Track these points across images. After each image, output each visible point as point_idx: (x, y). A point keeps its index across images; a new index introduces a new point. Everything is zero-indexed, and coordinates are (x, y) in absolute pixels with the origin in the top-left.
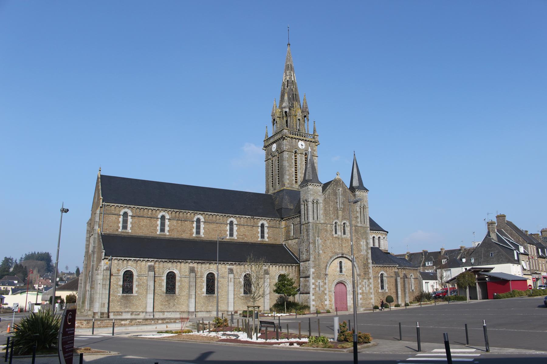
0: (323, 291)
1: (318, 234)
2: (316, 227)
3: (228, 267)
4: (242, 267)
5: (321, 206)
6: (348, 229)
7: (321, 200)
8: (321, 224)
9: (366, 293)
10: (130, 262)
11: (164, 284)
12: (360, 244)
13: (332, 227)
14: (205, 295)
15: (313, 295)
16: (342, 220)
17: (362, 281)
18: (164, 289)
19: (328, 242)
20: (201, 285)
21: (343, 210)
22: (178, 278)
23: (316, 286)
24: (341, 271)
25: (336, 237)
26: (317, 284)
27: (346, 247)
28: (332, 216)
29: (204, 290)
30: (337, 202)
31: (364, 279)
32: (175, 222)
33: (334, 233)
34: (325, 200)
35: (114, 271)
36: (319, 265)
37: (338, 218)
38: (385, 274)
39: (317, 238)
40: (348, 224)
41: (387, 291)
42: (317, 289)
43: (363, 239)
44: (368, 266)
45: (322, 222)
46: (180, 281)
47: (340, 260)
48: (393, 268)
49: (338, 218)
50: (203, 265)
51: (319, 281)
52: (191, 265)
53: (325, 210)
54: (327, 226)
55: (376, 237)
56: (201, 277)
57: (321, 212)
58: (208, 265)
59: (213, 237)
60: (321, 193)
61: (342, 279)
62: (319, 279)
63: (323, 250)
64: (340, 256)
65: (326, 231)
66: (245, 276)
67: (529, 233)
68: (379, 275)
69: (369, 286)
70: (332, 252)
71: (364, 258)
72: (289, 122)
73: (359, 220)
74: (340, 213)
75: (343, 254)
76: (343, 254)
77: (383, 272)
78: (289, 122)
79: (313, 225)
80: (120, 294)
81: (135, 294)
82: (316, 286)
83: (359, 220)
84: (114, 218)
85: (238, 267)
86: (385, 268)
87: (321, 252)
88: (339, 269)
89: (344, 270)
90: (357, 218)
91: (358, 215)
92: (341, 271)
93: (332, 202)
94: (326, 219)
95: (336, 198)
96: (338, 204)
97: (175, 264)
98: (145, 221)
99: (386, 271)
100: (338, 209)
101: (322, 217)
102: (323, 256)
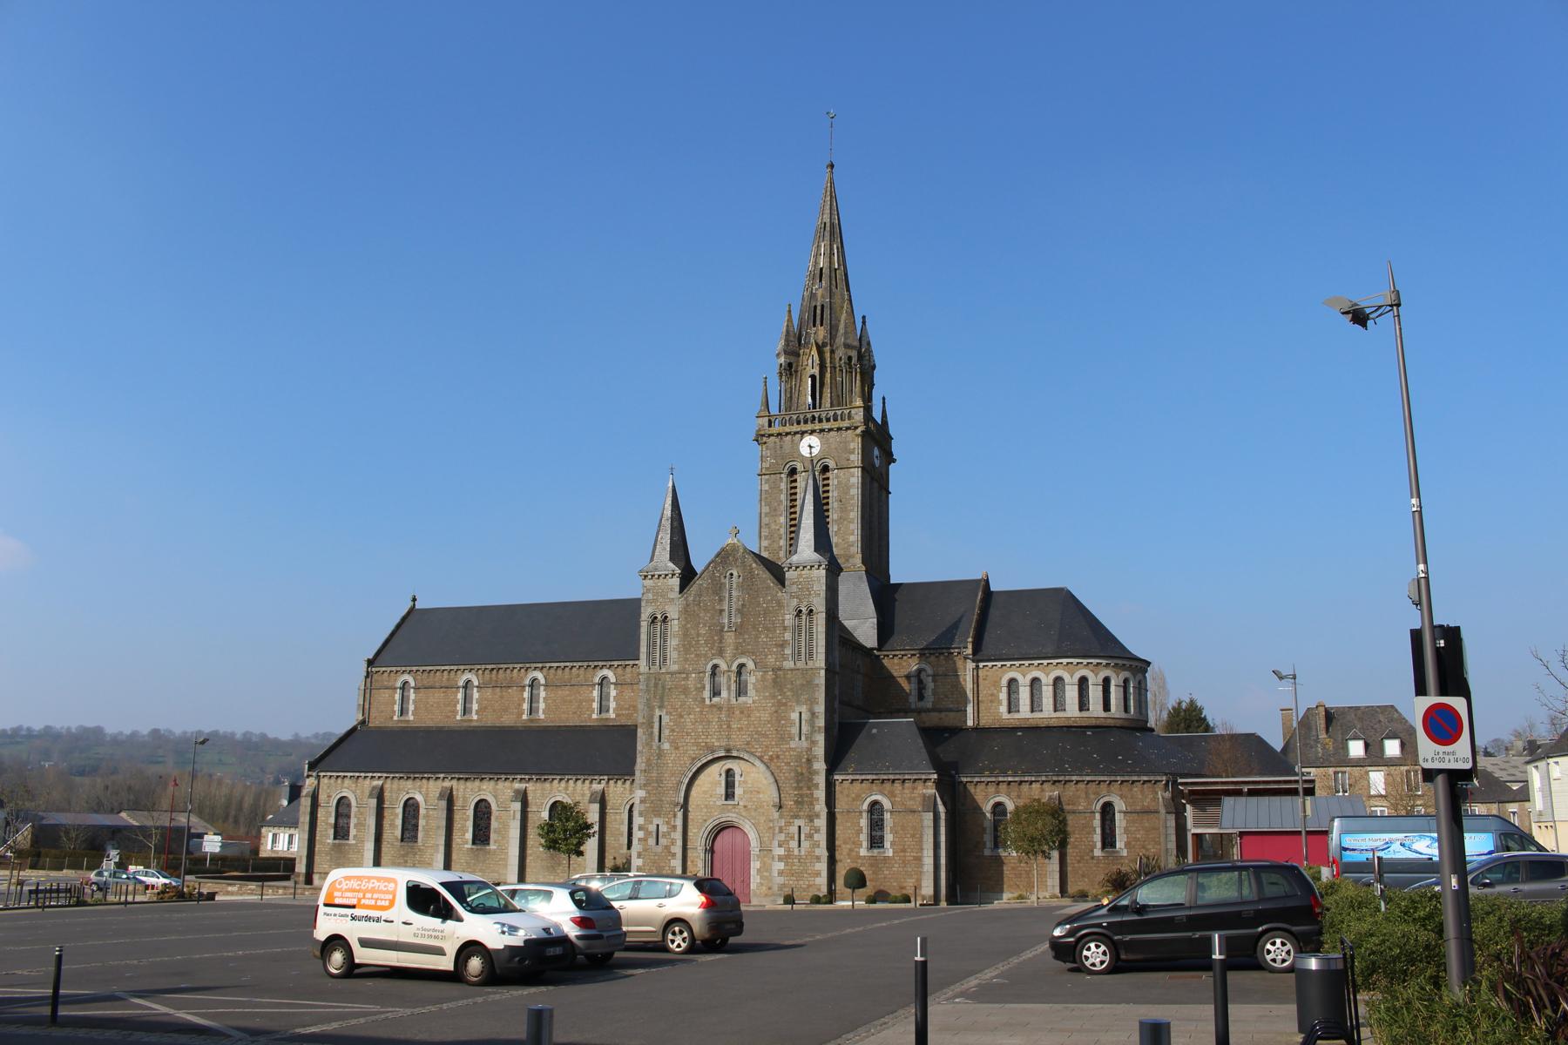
0: (667, 848)
1: (662, 699)
2: (656, 685)
3: (517, 785)
4: (547, 785)
5: (674, 626)
6: (751, 680)
7: (673, 612)
8: (672, 674)
9: (800, 858)
10: (347, 781)
11: (399, 822)
12: (788, 719)
13: (701, 680)
14: (469, 846)
15: (639, 856)
16: (735, 657)
17: (789, 824)
18: (398, 833)
19: (688, 720)
20: (464, 826)
21: (739, 630)
22: (422, 811)
23: (648, 833)
24: (729, 795)
25: (712, 706)
26: (652, 828)
27: (740, 729)
28: (704, 650)
29: (469, 836)
30: (722, 611)
31: (797, 817)
32: (488, 693)
33: (707, 694)
34: (686, 611)
35: (322, 797)
36: (659, 781)
37: (721, 653)
38: (1119, 805)
39: (657, 713)
40: (751, 665)
41: (890, 853)
42: (652, 841)
43: (798, 702)
44: (811, 780)
45: (675, 668)
46: (427, 816)
47: (729, 764)
48: (919, 785)
49: (721, 653)
50: (469, 784)
51: (656, 821)
52: (447, 784)
53: (685, 634)
54: (687, 679)
55: (1047, 680)
56: (464, 808)
57: (673, 642)
58: (477, 783)
59: (564, 716)
60: (675, 594)
61: (731, 816)
62: (659, 815)
63: (672, 742)
64: (722, 754)
65: (685, 691)
66: (477, 804)
67: (238, 736)
68: (865, 807)
69: (810, 836)
70: (697, 744)
71: (799, 757)
72: (831, 360)
73: (788, 651)
74: (730, 638)
75: (728, 750)
76: (728, 750)
77: (878, 797)
78: (831, 360)
79: (648, 679)
80: (330, 841)
81: (352, 841)
82: (648, 833)
83: (788, 651)
84: (386, 694)
85: (538, 784)
86: (888, 785)
87: (666, 746)
88: (722, 790)
89: (738, 791)
90: (782, 645)
91: (788, 636)
92: (729, 795)
93: (706, 611)
94: (686, 660)
95: (721, 600)
96: (726, 614)
97: (418, 783)
98: (436, 696)
99: (891, 796)
100: (722, 630)
101: (674, 655)
102: (670, 759)
